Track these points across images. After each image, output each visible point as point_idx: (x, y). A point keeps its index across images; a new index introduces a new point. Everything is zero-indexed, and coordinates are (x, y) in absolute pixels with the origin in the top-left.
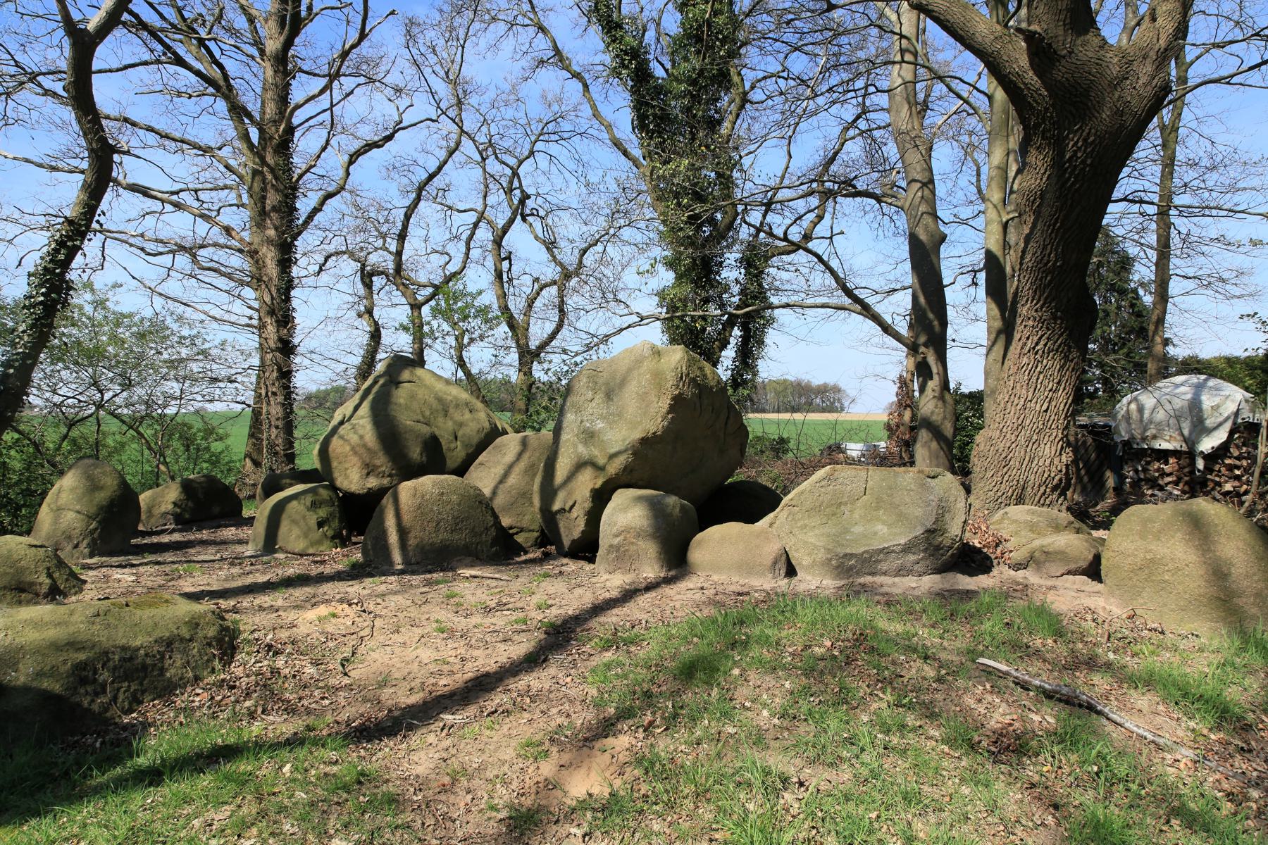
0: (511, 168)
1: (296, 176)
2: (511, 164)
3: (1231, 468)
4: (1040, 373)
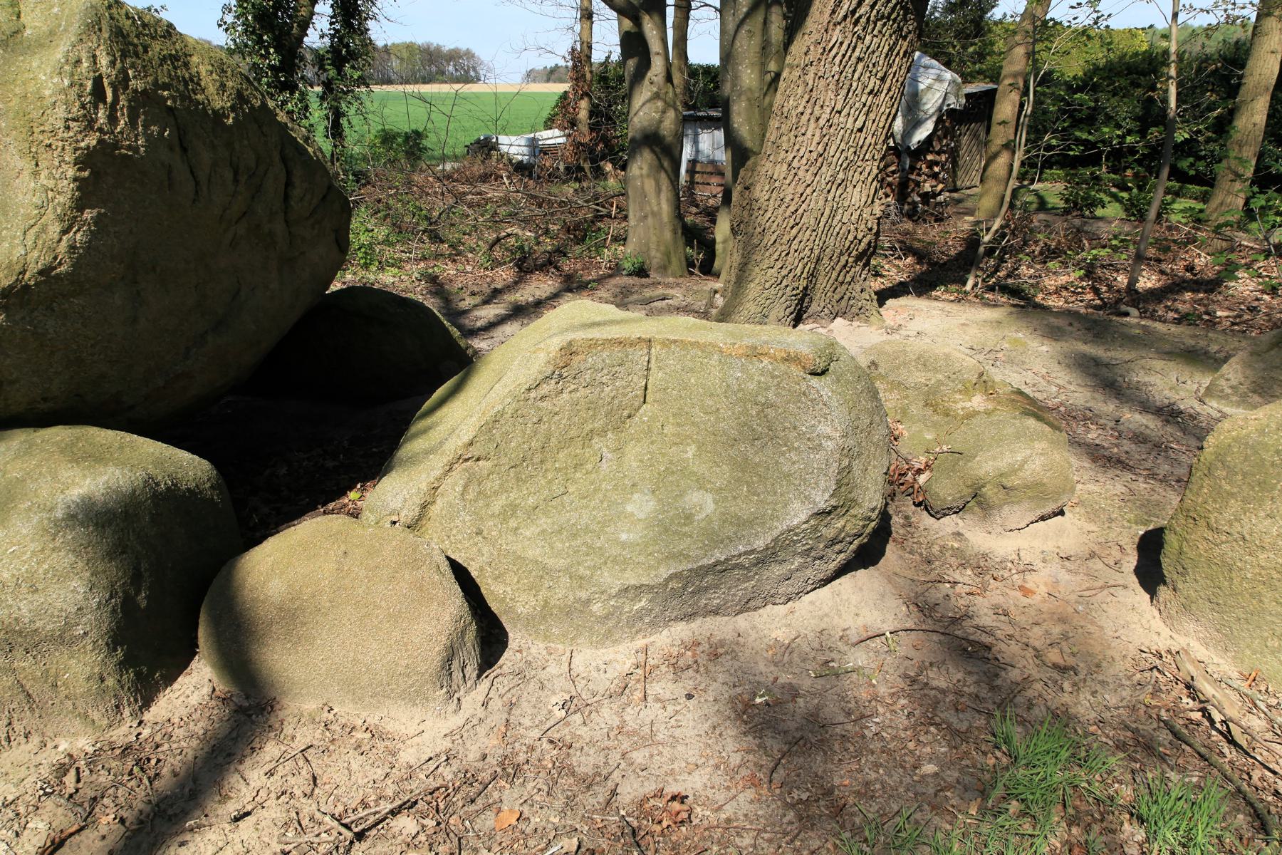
3: (931, 164)
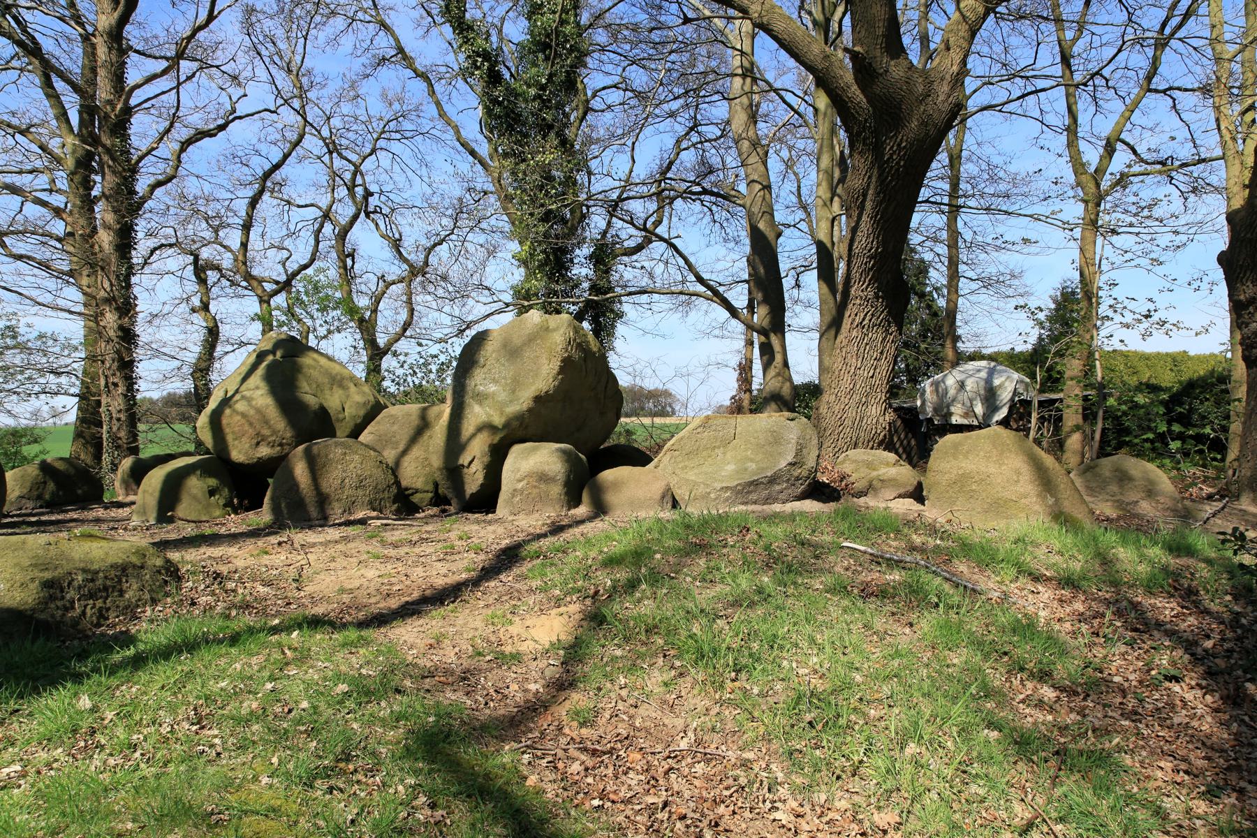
0: (354, 164)
1: (135, 158)
2: (354, 160)
4: (867, 344)
